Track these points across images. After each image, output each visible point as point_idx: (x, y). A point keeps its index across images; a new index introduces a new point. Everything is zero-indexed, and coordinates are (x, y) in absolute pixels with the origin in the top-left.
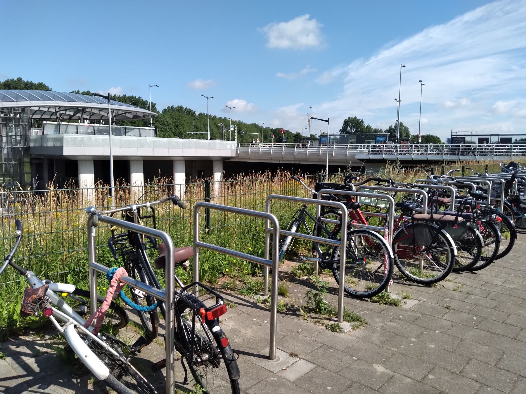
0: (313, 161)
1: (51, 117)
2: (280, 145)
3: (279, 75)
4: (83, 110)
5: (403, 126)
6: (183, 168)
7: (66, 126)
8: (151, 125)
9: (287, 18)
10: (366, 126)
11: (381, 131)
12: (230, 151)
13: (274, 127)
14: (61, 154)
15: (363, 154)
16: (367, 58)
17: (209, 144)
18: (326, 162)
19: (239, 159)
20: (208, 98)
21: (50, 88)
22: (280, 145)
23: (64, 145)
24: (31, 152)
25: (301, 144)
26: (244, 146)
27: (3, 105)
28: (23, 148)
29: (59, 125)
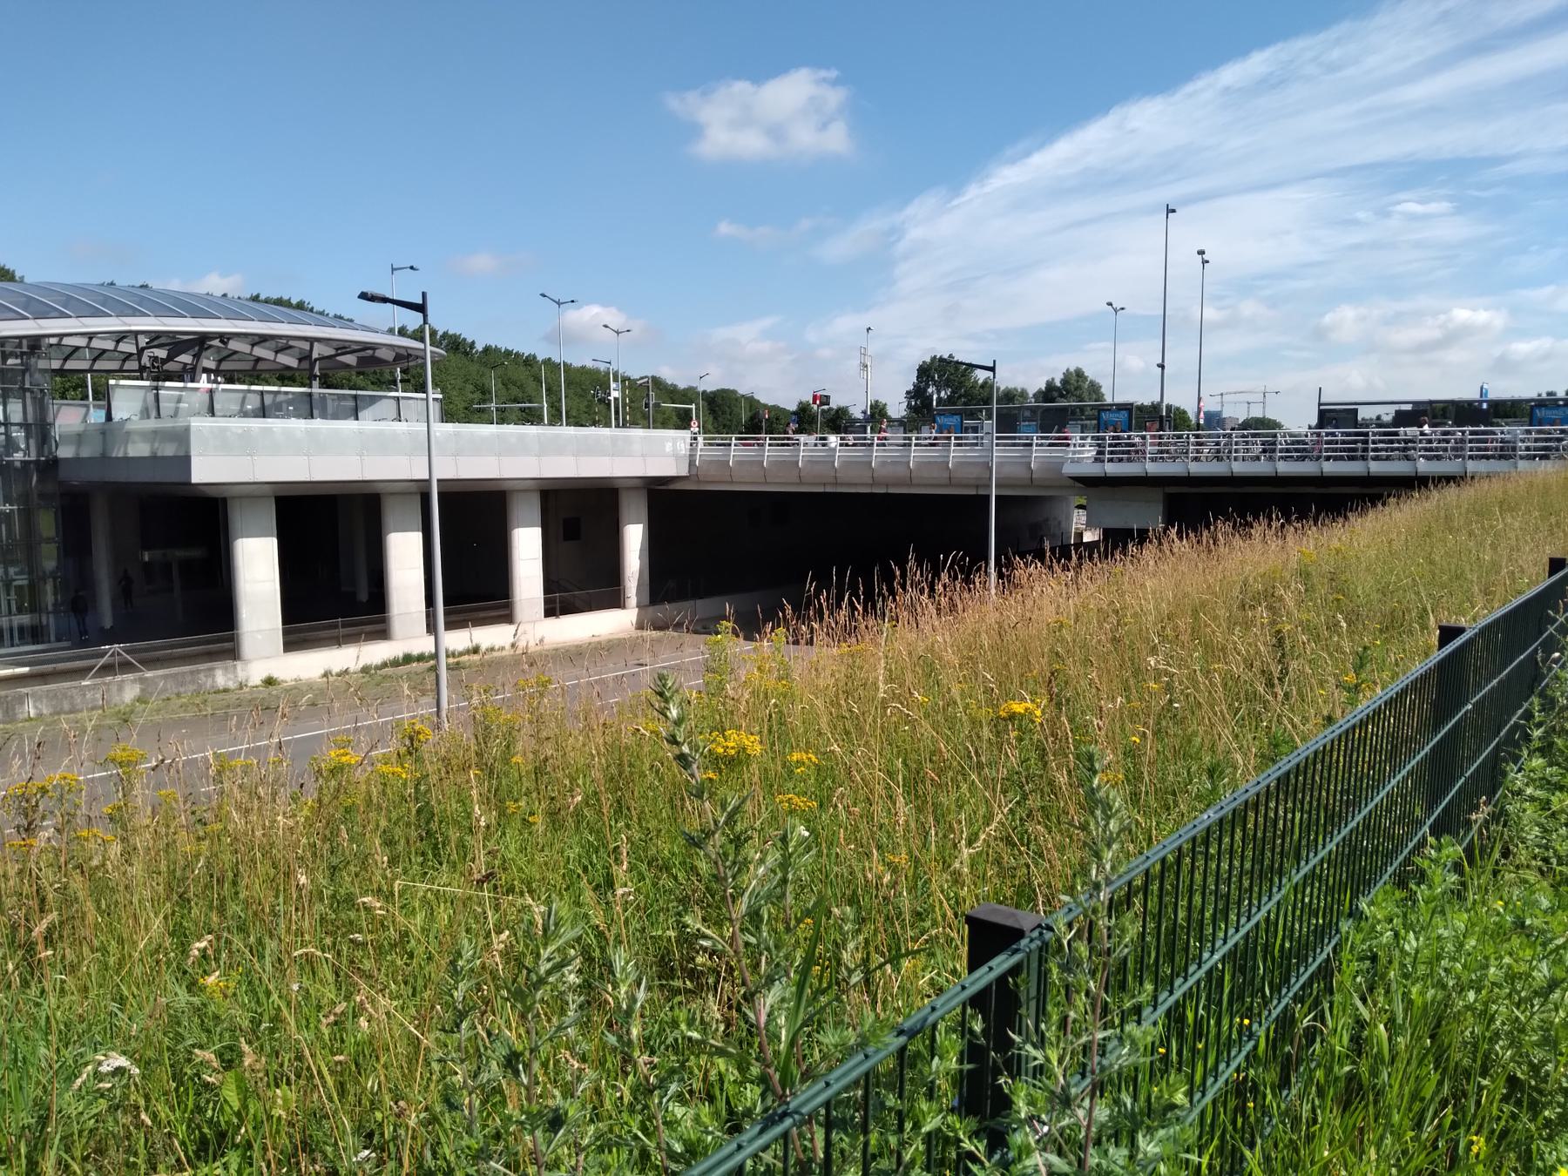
0: (926, 486)
1: (63, 364)
2: (1014, 438)
3: (725, 228)
4: (200, 342)
5: (1086, 378)
6: (644, 512)
7: (241, 395)
8: (400, 385)
9: (763, 70)
10: (980, 382)
11: (1023, 394)
12: (672, 461)
13: (709, 385)
14: (182, 480)
15: (1079, 461)
16: (956, 189)
17: (614, 439)
18: (990, 486)
19: (699, 482)
20: (559, 303)
21: (18, 275)
22: (1014, 438)
23: (193, 453)
24: (63, 474)
25: (851, 436)
26: (788, 445)
27: (41, 328)
28: (37, 462)
29: (157, 388)
